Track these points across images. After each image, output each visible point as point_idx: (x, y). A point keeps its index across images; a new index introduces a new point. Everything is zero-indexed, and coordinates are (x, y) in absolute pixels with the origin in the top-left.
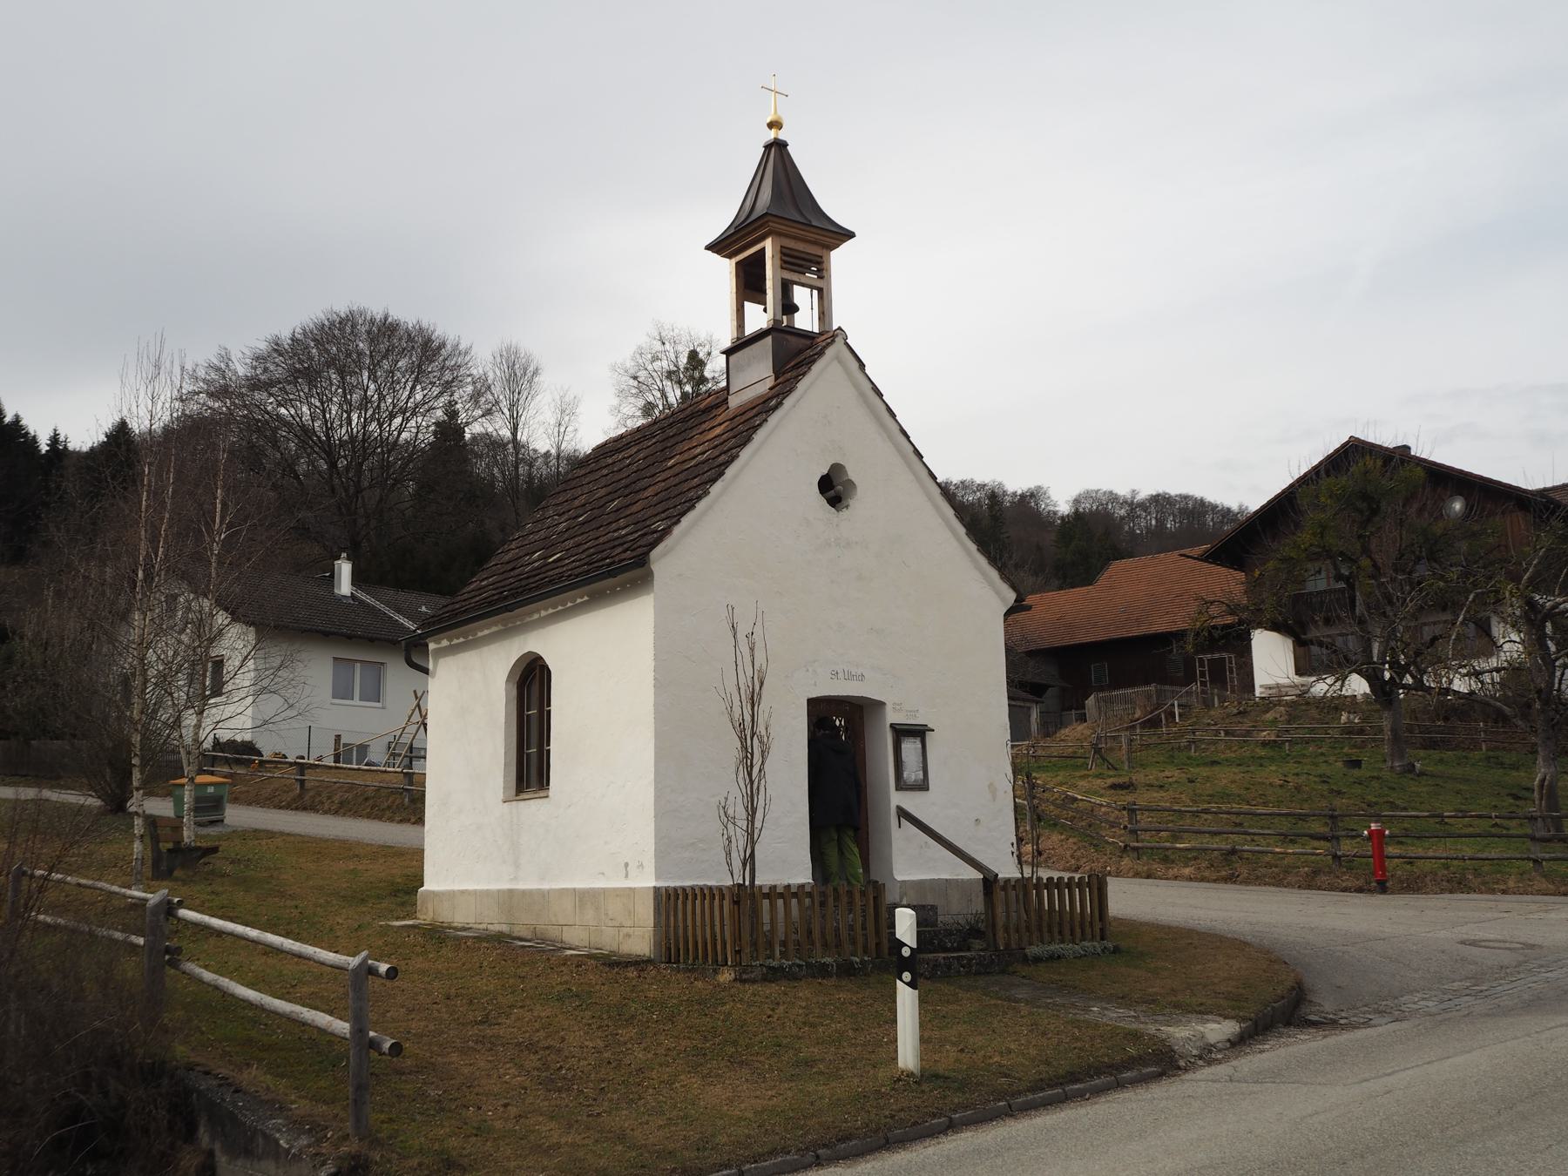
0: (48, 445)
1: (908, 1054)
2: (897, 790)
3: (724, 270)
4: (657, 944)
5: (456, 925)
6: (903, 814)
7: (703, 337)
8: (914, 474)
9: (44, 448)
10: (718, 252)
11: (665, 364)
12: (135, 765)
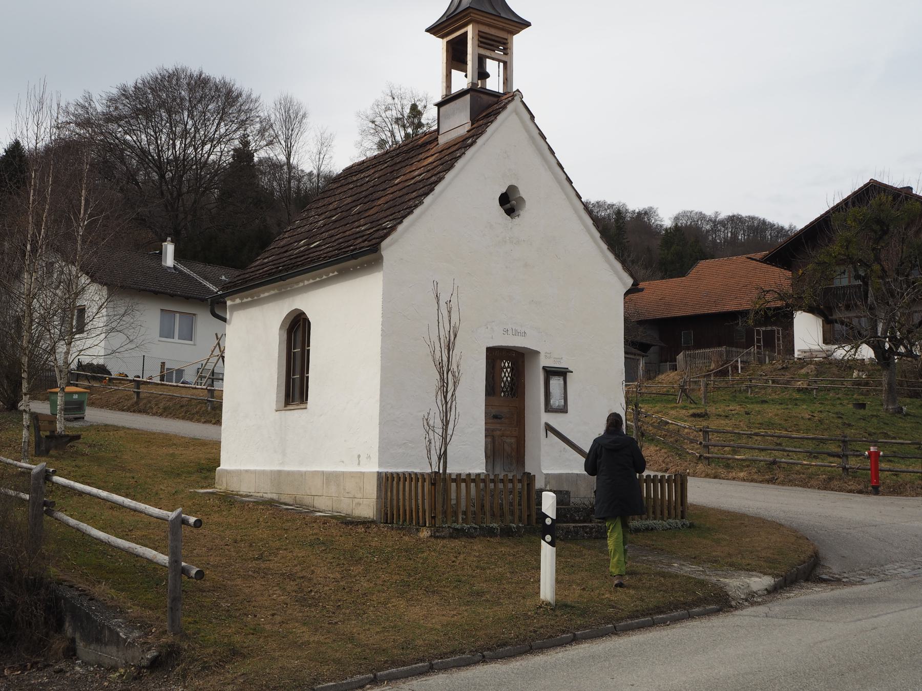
1: (547, 590)
3: (438, 46)
6: (549, 428)
10: (434, 34)
11: (394, 114)
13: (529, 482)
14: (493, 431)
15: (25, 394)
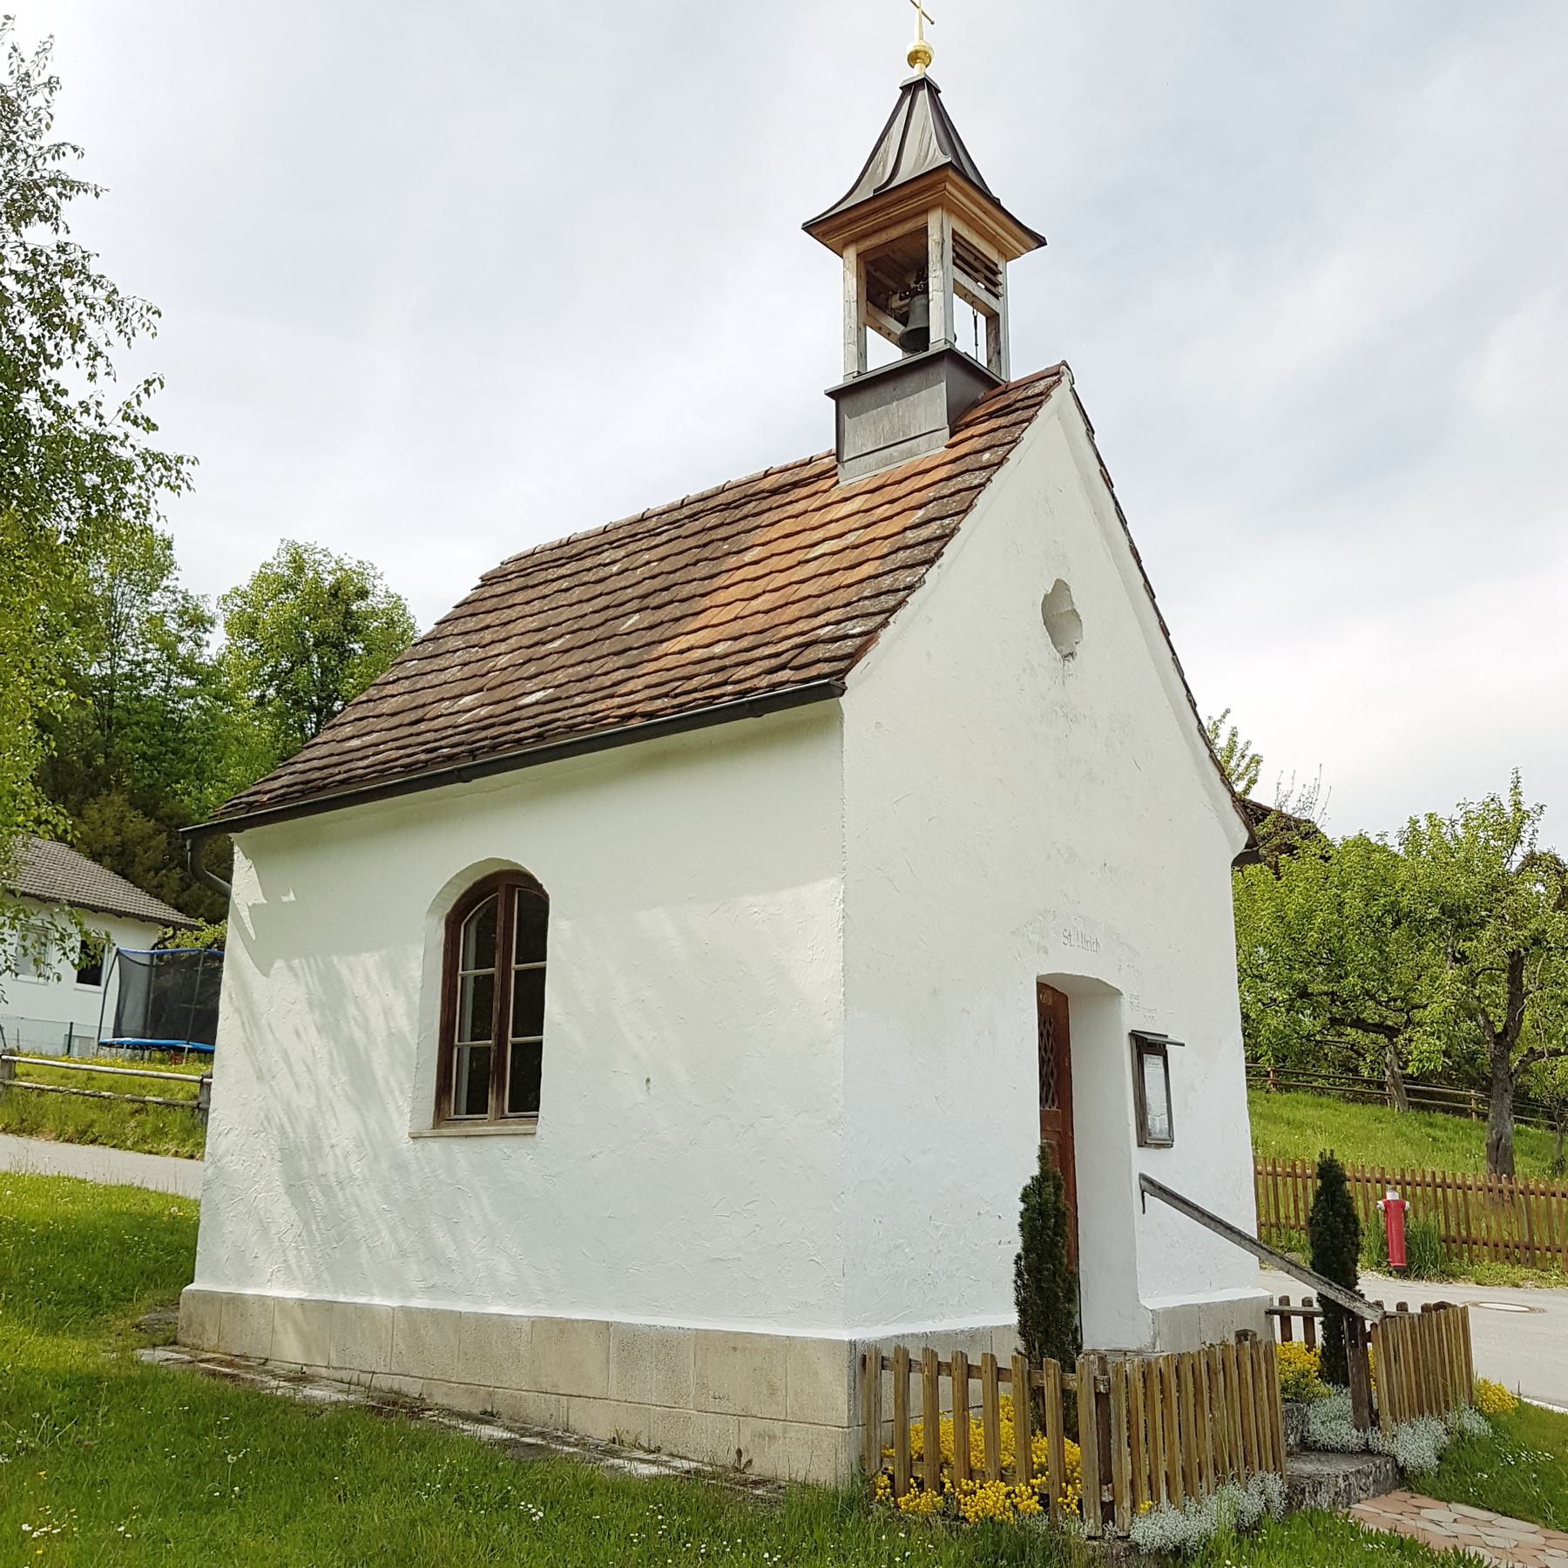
2: (1139, 1146)
6: (1151, 1187)
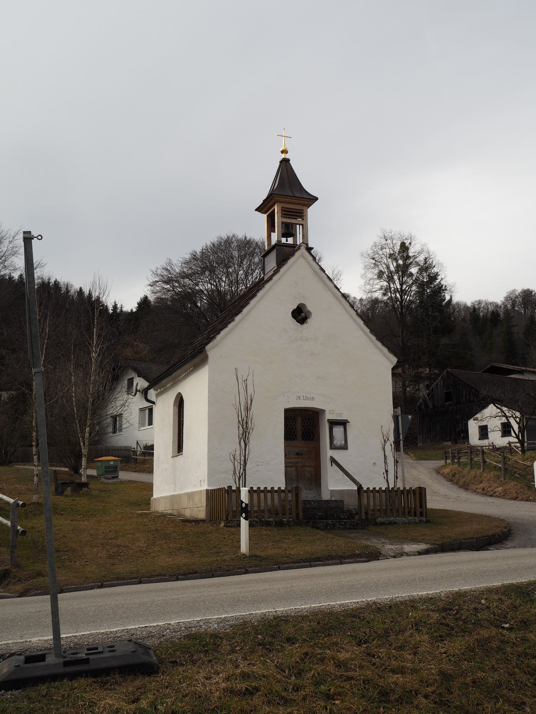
0: (112, 310)
1: (244, 547)
3: (263, 218)
4: (207, 514)
5: (160, 512)
6: (333, 461)
7: (407, 235)
8: (343, 305)
9: (111, 311)
10: (260, 211)
11: (388, 251)
12: (33, 445)
13: (297, 492)
14: (296, 463)
15: (35, 455)
